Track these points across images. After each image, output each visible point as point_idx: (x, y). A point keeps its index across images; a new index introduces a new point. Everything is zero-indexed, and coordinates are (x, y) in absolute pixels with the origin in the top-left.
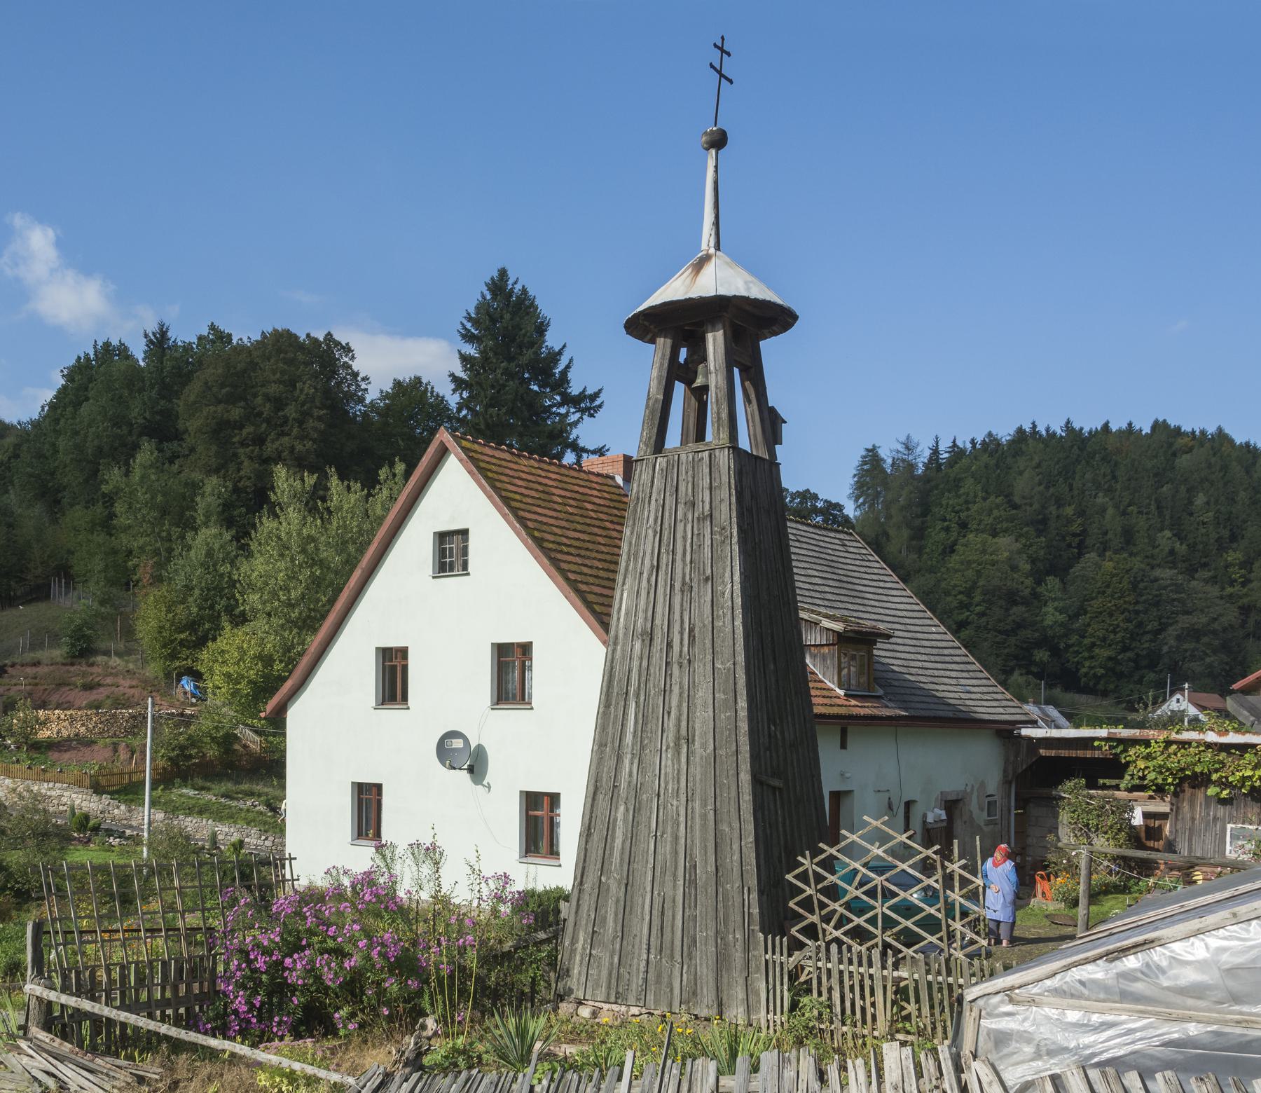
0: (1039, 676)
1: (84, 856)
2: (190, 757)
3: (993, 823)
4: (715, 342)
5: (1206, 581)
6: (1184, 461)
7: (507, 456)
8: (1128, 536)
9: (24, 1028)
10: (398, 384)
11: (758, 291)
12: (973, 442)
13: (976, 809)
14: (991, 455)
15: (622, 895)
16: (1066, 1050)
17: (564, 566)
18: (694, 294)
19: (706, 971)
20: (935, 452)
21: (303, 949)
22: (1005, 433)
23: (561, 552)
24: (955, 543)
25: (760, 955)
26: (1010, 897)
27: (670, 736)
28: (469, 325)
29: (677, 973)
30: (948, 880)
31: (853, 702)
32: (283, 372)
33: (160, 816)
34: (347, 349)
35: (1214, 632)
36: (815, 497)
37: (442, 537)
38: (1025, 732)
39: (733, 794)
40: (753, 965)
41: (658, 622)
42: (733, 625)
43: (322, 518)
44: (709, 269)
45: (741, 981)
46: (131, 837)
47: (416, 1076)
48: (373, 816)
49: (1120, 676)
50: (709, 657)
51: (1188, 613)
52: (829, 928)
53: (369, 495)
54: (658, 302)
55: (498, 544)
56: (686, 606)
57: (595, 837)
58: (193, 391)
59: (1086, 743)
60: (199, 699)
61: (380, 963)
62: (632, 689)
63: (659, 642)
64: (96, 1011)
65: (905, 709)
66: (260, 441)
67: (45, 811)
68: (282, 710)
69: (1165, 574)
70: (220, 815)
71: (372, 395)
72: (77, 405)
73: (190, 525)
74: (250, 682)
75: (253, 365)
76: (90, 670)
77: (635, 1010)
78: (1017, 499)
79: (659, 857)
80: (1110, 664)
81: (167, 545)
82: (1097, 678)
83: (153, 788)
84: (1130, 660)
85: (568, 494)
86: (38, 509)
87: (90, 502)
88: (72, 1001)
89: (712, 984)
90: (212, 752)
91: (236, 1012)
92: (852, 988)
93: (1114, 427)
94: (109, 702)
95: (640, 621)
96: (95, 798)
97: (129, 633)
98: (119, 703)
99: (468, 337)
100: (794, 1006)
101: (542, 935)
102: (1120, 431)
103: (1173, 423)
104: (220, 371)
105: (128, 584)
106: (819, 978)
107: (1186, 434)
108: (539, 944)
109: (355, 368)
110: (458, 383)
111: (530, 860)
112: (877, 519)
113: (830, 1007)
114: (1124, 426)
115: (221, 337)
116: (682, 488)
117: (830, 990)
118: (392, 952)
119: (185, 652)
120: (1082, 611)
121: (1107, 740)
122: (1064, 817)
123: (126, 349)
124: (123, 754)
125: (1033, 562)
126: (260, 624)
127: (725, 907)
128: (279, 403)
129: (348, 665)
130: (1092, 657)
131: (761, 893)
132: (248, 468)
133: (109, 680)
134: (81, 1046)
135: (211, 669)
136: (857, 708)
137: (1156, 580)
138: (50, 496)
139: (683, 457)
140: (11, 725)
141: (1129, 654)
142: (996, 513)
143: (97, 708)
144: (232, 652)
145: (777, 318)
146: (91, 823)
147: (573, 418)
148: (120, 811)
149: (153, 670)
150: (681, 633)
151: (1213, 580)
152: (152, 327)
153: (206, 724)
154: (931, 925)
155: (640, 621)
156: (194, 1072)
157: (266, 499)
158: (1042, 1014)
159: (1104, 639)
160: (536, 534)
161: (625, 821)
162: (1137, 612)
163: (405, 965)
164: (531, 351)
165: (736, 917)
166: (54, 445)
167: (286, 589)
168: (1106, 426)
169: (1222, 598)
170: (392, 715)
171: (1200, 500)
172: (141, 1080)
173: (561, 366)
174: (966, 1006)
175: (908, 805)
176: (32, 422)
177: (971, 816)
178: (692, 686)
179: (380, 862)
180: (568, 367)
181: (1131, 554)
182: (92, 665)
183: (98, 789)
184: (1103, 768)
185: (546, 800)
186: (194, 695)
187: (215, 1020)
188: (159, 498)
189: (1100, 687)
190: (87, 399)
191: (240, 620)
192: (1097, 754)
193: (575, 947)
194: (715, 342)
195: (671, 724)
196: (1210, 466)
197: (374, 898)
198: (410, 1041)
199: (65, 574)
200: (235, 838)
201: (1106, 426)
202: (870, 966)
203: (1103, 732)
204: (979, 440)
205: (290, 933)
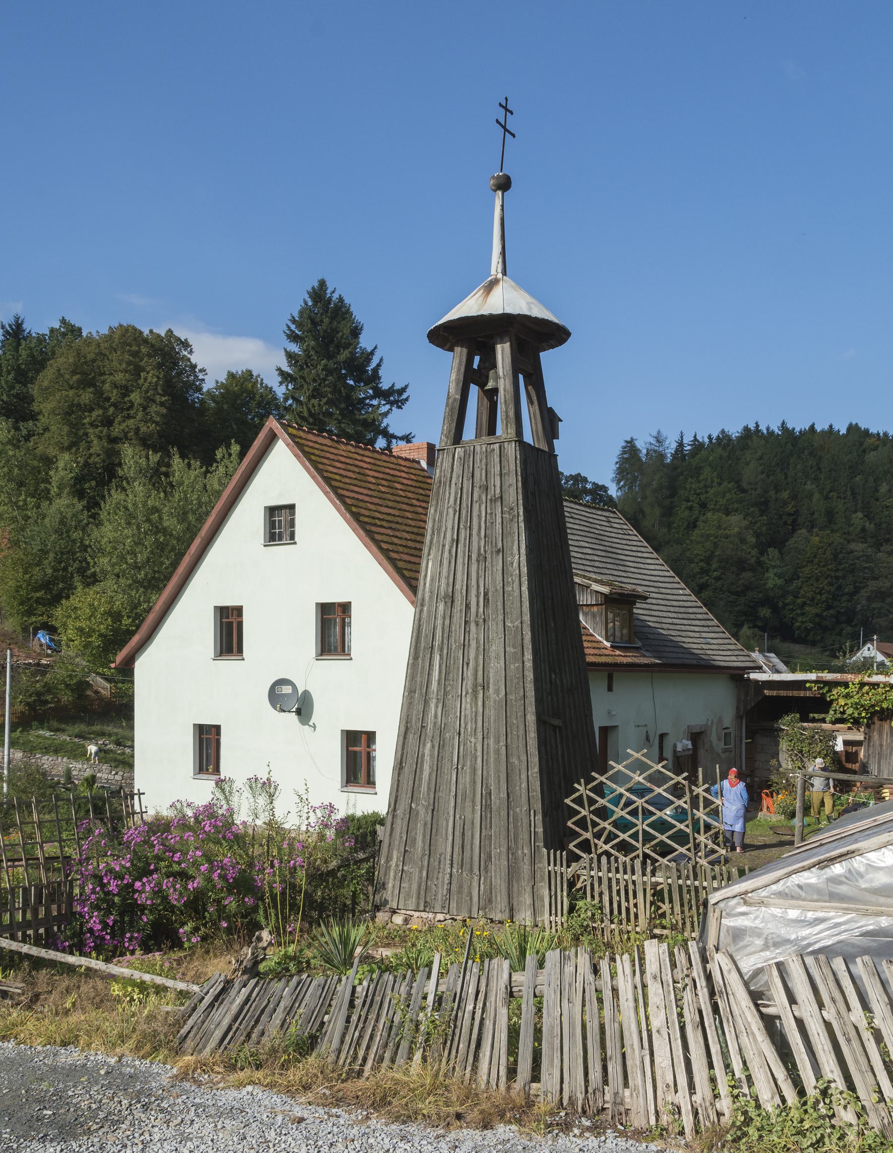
0: (763, 629)
2: (47, 702)
4: (503, 352)
7: (328, 442)
8: (830, 515)
11: (538, 311)
12: (710, 437)
13: (715, 740)
14: (724, 448)
15: (429, 819)
16: (788, 941)
17: (378, 537)
18: (485, 312)
20: (681, 444)
21: (151, 873)
23: (375, 525)
24: (697, 520)
27: (469, 684)
28: (293, 327)
29: (475, 884)
31: (618, 652)
33: (19, 755)
34: (186, 344)
36: (585, 480)
38: (754, 676)
39: (522, 732)
40: (538, 875)
41: (458, 587)
42: (520, 590)
44: (498, 291)
47: (253, 982)
48: (212, 752)
50: (501, 617)
51: (876, 579)
52: (600, 843)
53: (207, 471)
54: (456, 317)
55: (321, 518)
56: (482, 573)
57: (406, 770)
58: (46, 377)
59: (800, 685)
60: (54, 650)
61: (219, 883)
62: (437, 644)
63: (459, 605)
65: (659, 658)
68: (130, 661)
69: (858, 547)
71: (208, 385)
74: (101, 635)
77: (440, 917)
78: (745, 485)
79: (460, 786)
80: (817, 619)
82: (808, 631)
83: (12, 731)
84: (832, 616)
85: (381, 476)
90: (66, 698)
91: (91, 931)
92: (618, 892)
93: (818, 428)
100: (572, 909)
102: (823, 431)
103: (863, 426)
104: (71, 360)
106: (592, 885)
107: (872, 435)
109: (193, 361)
111: (350, 789)
113: (601, 908)
114: (826, 428)
117: (601, 894)
118: (231, 874)
121: (816, 682)
122: (784, 745)
125: (758, 535)
126: (109, 584)
127: (515, 827)
129: (188, 623)
130: (803, 614)
137: (852, 552)
139: (478, 448)
141: (832, 612)
142: (728, 496)
145: (552, 334)
150: (478, 596)
153: (61, 673)
154: (681, 838)
155: (443, 586)
156: (53, 985)
159: (813, 599)
160: (354, 509)
161: (431, 756)
162: (837, 578)
163: (243, 885)
167: (134, 553)
168: (812, 427)
170: (229, 665)
173: (373, 364)
175: (662, 737)
178: (486, 640)
180: (379, 365)
181: (832, 531)
184: (813, 705)
185: (364, 737)
186: (49, 647)
187: (72, 938)
188: (16, 471)
189: (810, 638)
191: (92, 580)
192: (808, 694)
193: (391, 863)
194: (503, 352)
195: (469, 673)
197: (215, 827)
198: (248, 952)
201: (812, 427)
202: (633, 873)
203: (812, 676)
205: (139, 859)
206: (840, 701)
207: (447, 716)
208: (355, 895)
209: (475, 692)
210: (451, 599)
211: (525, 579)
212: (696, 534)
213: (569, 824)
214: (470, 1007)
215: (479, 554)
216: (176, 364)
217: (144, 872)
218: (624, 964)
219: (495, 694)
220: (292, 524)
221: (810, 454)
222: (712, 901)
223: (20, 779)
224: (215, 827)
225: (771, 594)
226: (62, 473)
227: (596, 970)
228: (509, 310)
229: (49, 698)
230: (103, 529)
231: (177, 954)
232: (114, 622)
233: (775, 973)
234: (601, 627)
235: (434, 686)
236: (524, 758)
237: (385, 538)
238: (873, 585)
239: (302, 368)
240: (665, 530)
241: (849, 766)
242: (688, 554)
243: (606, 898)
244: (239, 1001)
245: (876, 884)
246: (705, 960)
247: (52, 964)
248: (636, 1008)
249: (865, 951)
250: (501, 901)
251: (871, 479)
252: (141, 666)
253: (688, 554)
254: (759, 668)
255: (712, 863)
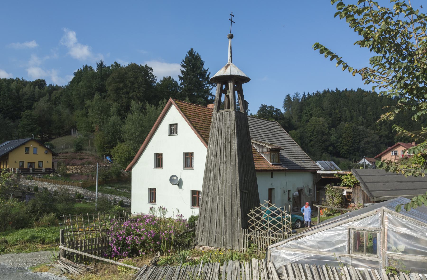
0: (330, 154)
1: (78, 206)
2: (109, 178)
3: (311, 195)
4: (231, 85)
5: (371, 129)
6: (365, 99)
7: (187, 105)
8: (352, 117)
9: (59, 257)
10: (165, 78)
11: (241, 74)
12: (313, 93)
13: (306, 192)
14: (318, 97)
15: (210, 219)
16: (288, 260)
17: (201, 133)
18: (225, 74)
19: (229, 238)
20: (304, 96)
21: (131, 235)
22: (321, 91)
23: (201, 130)
24: (309, 119)
25: (242, 234)
26: (310, 216)
27: (221, 180)
28: (183, 63)
29: (223, 238)
30: (283, 215)
31: (274, 166)
32: (134, 75)
33: (100, 194)
34: (151, 69)
35: (373, 142)
36: (274, 108)
37: (171, 125)
38: (318, 172)
39: (235, 195)
40: (240, 236)
41: (218, 152)
42: (235, 153)
43: (144, 114)
44: (229, 68)
45: (237, 240)
46: (92, 200)
47: (154, 267)
48: (154, 197)
49: (350, 153)
50: (230, 161)
51: (367, 137)
52: (257, 227)
53: (157, 108)
54: (217, 76)
55: (185, 127)
56: (225, 149)
57: (203, 205)
58: (110, 79)
59: (332, 175)
60: (111, 162)
61: (150, 238)
62: (212, 169)
63: (218, 158)
64: (77, 252)
65: (287, 167)
66: (128, 93)
67: (69, 194)
68: (130, 169)
69: (361, 127)
70: (117, 194)
71: (158, 81)
72: (78, 82)
73: (108, 115)
74: (125, 158)
75: (126, 73)
76: (81, 154)
77: (213, 248)
78: (324, 108)
79: (218, 210)
80: (348, 150)
81: (103, 121)
82: (345, 154)
83: (98, 187)
84: (352, 149)
85: (203, 114)
86: (68, 110)
87: (82, 109)
88: (71, 250)
89: (231, 241)
90: (115, 177)
91: (114, 251)
92: (262, 242)
93: (348, 90)
94: (87, 163)
95: (214, 152)
96: (82, 189)
97: (92, 144)
98: (90, 163)
99: (183, 66)
100: (249, 246)
101: (191, 230)
102: (349, 91)
103: (362, 89)
104: (117, 74)
105: (92, 131)
106: (255, 239)
107: (365, 92)
108: (190, 232)
109: (153, 74)
110: (181, 78)
111: (193, 208)
112: (290, 113)
113: (257, 246)
114: (350, 90)
115: (117, 65)
116: (223, 120)
117: (257, 242)
118: (153, 235)
119: (107, 150)
120: (341, 137)
121: (337, 174)
122: (327, 194)
123: (92, 68)
124: (90, 178)
125: (328, 124)
126: (128, 142)
127: (234, 222)
128: (133, 83)
129: (147, 159)
130: (343, 149)
131: (242, 219)
132: (125, 100)
133: (87, 157)
134: (73, 261)
135: (114, 154)
136: (275, 168)
137: (358, 129)
138: (71, 107)
139: (224, 113)
140: (60, 170)
141: (352, 148)
142: (319, 112)
143: (83, 165)
144: (120, 148)
145: (246, 80)
146: (81, 196)
147: (211, 87)
148: (89, 193)
149: (98, 154)
150: (223, 155)
151: (373, 129)
152: (99, 62)
153: (113, 169)
154: (280, 226)
155: (214, 152)
156: (102, 267)
157: (129, 109)
158: (285, 252)
159: (346, 144)
160: (194, 125)
161: (210, 201)
162: (354, 137)
163: (156, 238)
164: (199, 70)
165: (236, 225)
166: (72, 93)
167: (134, 133)
168: (346, 89)
169: (375, 133)
170: (158, 171)
171: (369, 108)
172: (88, 269)
173: (208, 74)
174: (268, 250)
175: (289, 191)
176: (66, 86)
177: (305, 194)
178: (226, 168)
179: (151, 212)
180: (209, 74)
181: (352, 122)
182: (82, 153)
183: (83, 187)
184: (337, 181)
185: (197, 192)
186: (110, 161)
187: (108, 253)
188: (100, 108)
189: (345, 156)
190: (81, 81)
191: (122, 141)
192: (335, 177)
193: (199, 232)
194: (231, 85)
195: (221, 177)
196: (371, 100)
197: (150, 220)
198: (154, 258)
199: (75, 128)
200: (121, 199)
201: (346, 89)
202: (266, 236)
203: (336, 172)
204: (315, 93)
205: (128, 231)
206: (345, 180)
207: (215, 189)
208: (189, 241)
209: (223, 183)
210: (216, 156)
211: (236, 150)
212: (309, 124)
213: (249, 221)
214: (209, 276)
215: (224, 143)
216: (148, 75)
217: (129, 234)
218: (247, 264)
219: (228, 184)
220: (177, 129)
221: (345, 98)
222: (269, 248)
223: (100, 202)
224: (149, 221)
225: (333, 142)
226: (114, 109)
227: (241, 266)
228: (232, 74)
229: (110, 177)
230: (126, 126)
231: (137, 258)
232: (129, 154)
233: (284, 268)
234: (269, 159)
235: (211, 181)
236: (236, 202)
237: (203, 134)
238: (366, 139)
239: (186, 76)
240: (299, 123)
241: (349, 200)
242: (306, 130)
243: (259, 243)
244: (150, 273)
245: (309, 245)
246: (266, 264)
247: (102, 261)
248: (250, 277)
249: (306, 263)
250: (230, 244)
251: (365, 106)
252: (134, 170)
253: (306, 130)
254: (320, 169)
255: (288, 233)
